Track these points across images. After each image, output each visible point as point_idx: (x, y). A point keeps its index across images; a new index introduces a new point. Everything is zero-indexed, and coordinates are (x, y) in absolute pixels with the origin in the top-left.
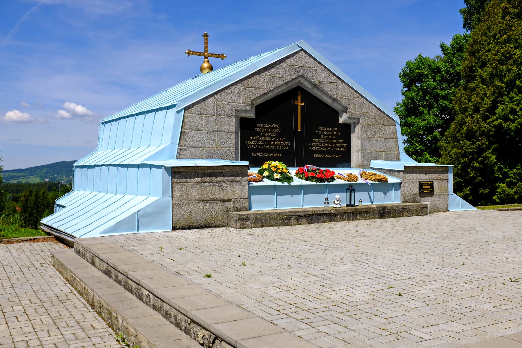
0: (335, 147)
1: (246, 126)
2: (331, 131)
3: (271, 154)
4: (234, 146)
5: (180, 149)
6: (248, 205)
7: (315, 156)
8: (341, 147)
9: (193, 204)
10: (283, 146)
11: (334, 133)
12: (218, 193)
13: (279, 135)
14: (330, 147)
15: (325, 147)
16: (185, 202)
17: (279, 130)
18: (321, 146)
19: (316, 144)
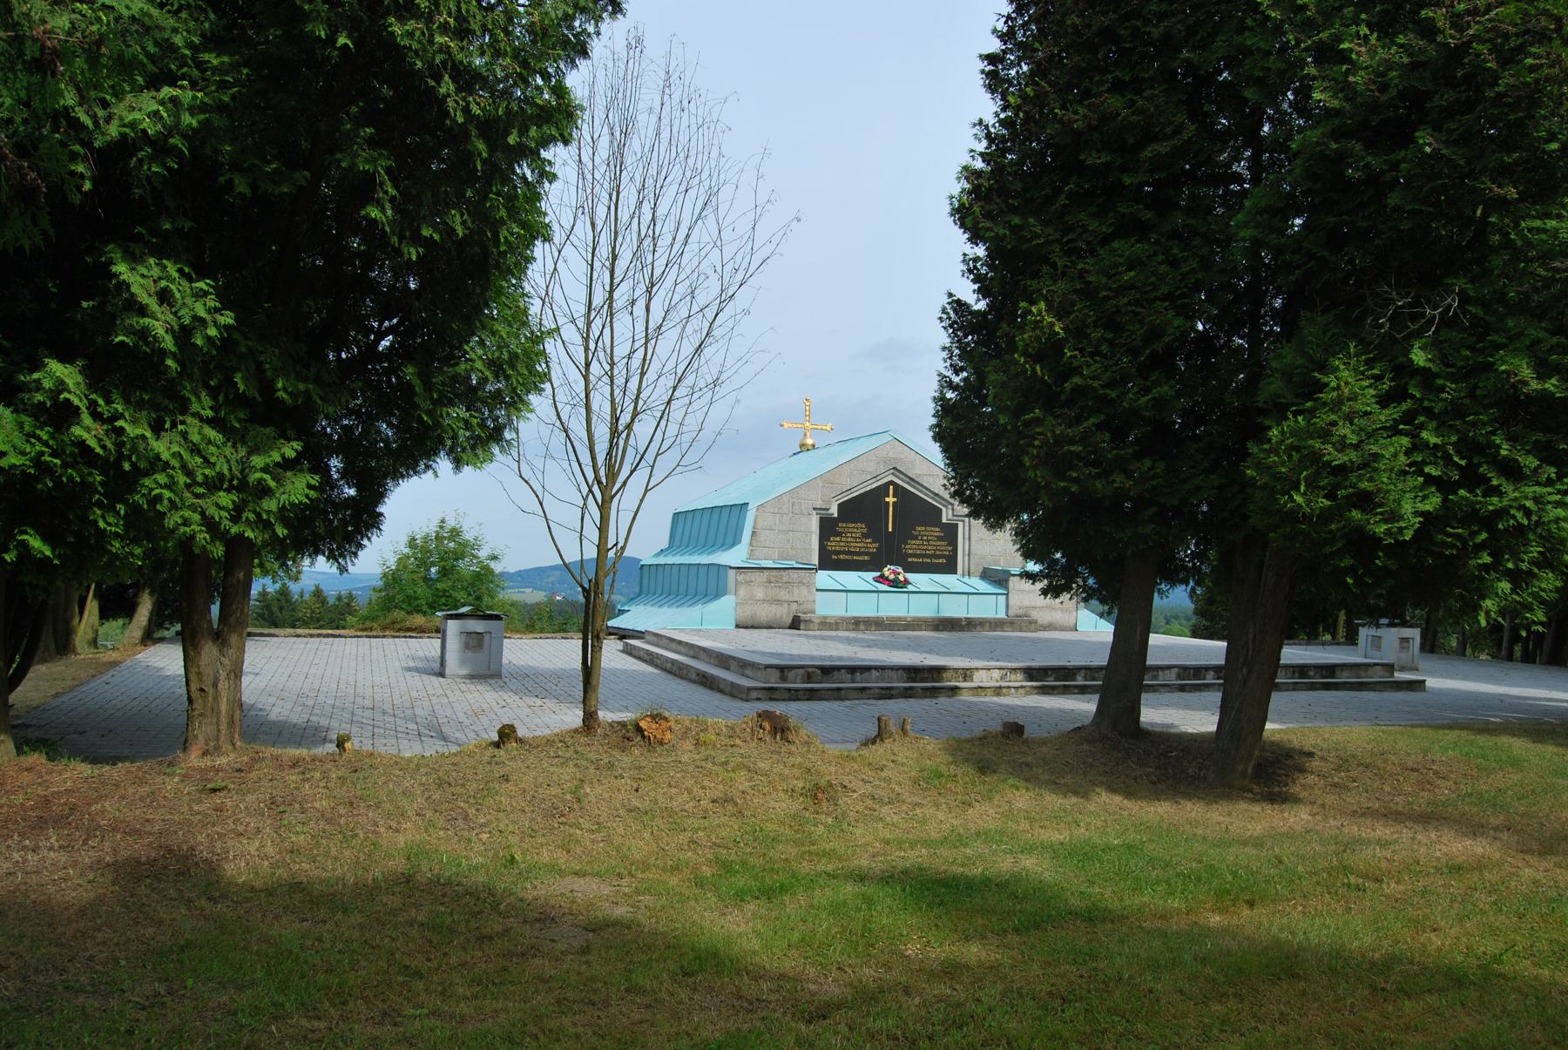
1: (828, 527)
12: (783, 595)
13: (865, 536)
19: (911, 547)
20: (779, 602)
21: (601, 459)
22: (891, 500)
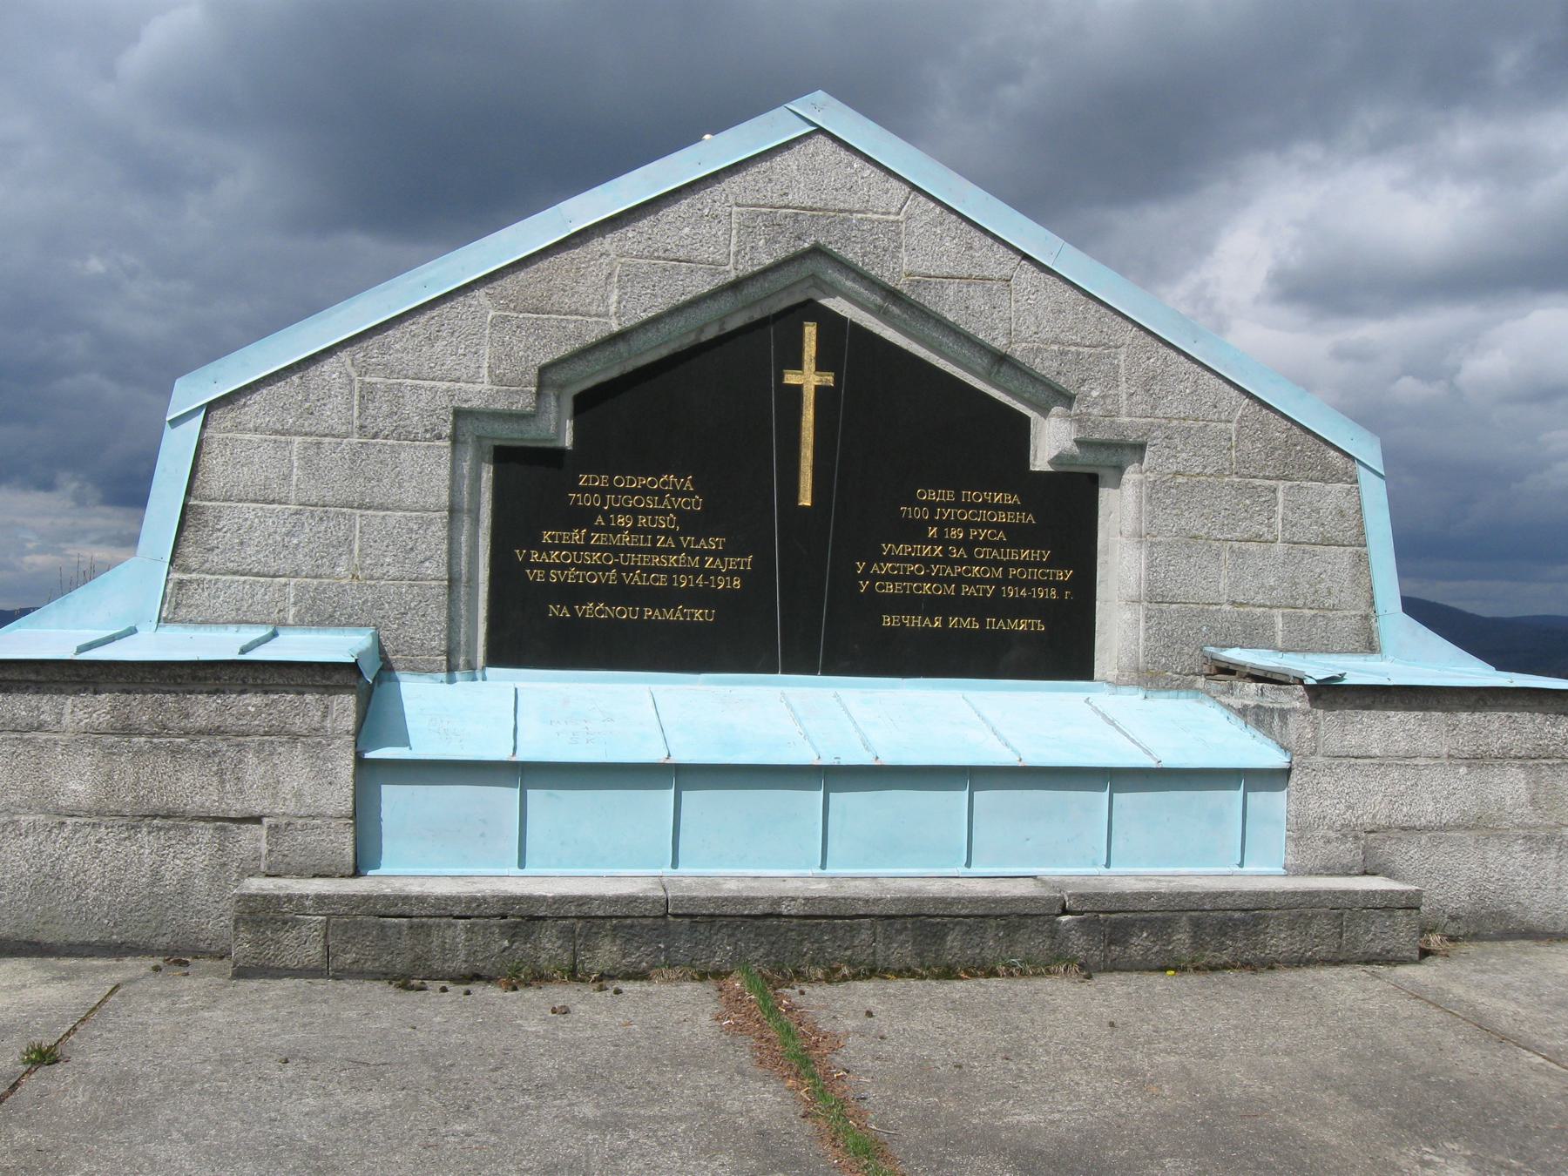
0: (1005, 581)
1: (528, 486)
2: (985, 505)
3: (648, 612)
4: (443, 572)
5: (181, 584)
6: (349, 850)
7: (887, 621)
8: (1039, 583)
9: (67, 832)
10: (717, 572)
11: (1002, 517)
12: (192, 786)
13: (689, 523)
14: (973, 582)
15: (948, 580)
16: (25, 820)
17: (696, 503)
18: (928, 578)
19: (895, 569)
20: (172, 818)
21: (1477, 673)
22: (808, 379)
